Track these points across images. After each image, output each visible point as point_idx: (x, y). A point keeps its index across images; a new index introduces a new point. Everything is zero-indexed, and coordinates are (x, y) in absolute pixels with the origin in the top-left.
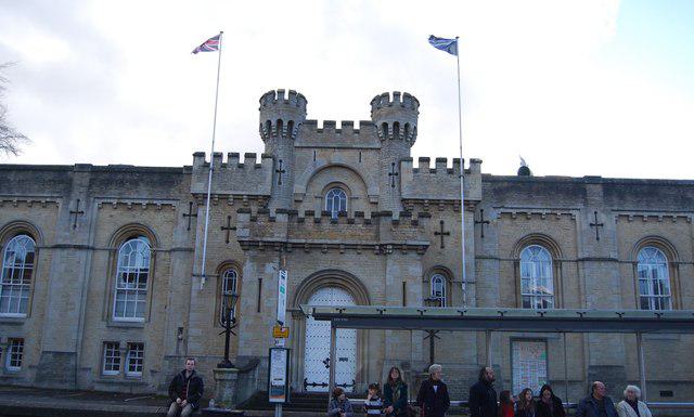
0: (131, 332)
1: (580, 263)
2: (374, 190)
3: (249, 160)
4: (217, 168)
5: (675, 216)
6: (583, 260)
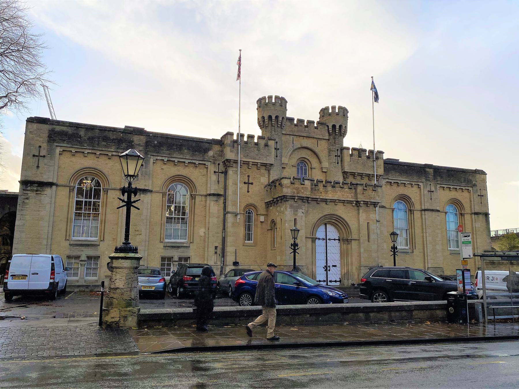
0: (180, 250)
1: (423, 212)
2: (325, 164)
3: (250, 139)
4: (243, 143)
5: (110, 154)
6: (425, 210)
